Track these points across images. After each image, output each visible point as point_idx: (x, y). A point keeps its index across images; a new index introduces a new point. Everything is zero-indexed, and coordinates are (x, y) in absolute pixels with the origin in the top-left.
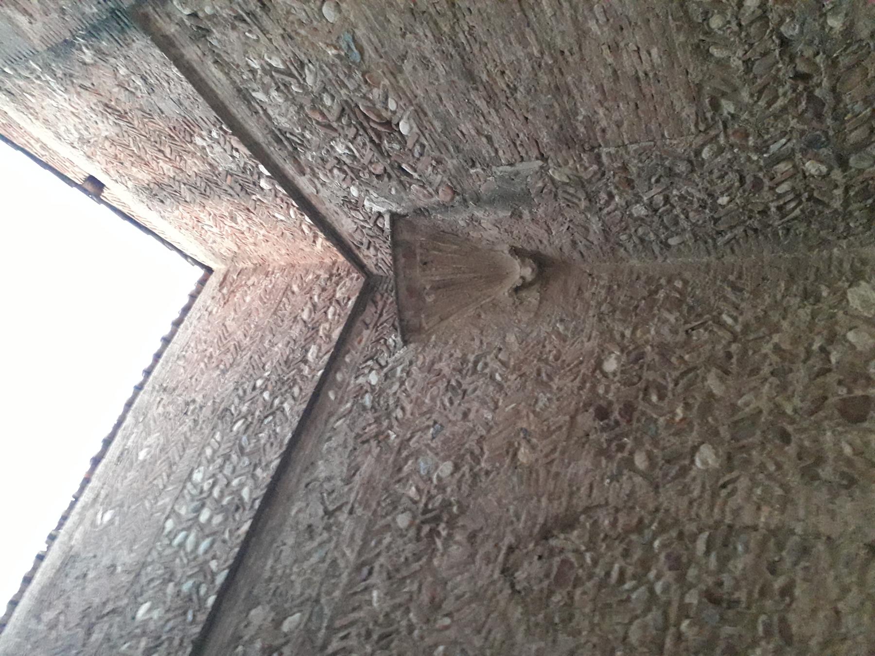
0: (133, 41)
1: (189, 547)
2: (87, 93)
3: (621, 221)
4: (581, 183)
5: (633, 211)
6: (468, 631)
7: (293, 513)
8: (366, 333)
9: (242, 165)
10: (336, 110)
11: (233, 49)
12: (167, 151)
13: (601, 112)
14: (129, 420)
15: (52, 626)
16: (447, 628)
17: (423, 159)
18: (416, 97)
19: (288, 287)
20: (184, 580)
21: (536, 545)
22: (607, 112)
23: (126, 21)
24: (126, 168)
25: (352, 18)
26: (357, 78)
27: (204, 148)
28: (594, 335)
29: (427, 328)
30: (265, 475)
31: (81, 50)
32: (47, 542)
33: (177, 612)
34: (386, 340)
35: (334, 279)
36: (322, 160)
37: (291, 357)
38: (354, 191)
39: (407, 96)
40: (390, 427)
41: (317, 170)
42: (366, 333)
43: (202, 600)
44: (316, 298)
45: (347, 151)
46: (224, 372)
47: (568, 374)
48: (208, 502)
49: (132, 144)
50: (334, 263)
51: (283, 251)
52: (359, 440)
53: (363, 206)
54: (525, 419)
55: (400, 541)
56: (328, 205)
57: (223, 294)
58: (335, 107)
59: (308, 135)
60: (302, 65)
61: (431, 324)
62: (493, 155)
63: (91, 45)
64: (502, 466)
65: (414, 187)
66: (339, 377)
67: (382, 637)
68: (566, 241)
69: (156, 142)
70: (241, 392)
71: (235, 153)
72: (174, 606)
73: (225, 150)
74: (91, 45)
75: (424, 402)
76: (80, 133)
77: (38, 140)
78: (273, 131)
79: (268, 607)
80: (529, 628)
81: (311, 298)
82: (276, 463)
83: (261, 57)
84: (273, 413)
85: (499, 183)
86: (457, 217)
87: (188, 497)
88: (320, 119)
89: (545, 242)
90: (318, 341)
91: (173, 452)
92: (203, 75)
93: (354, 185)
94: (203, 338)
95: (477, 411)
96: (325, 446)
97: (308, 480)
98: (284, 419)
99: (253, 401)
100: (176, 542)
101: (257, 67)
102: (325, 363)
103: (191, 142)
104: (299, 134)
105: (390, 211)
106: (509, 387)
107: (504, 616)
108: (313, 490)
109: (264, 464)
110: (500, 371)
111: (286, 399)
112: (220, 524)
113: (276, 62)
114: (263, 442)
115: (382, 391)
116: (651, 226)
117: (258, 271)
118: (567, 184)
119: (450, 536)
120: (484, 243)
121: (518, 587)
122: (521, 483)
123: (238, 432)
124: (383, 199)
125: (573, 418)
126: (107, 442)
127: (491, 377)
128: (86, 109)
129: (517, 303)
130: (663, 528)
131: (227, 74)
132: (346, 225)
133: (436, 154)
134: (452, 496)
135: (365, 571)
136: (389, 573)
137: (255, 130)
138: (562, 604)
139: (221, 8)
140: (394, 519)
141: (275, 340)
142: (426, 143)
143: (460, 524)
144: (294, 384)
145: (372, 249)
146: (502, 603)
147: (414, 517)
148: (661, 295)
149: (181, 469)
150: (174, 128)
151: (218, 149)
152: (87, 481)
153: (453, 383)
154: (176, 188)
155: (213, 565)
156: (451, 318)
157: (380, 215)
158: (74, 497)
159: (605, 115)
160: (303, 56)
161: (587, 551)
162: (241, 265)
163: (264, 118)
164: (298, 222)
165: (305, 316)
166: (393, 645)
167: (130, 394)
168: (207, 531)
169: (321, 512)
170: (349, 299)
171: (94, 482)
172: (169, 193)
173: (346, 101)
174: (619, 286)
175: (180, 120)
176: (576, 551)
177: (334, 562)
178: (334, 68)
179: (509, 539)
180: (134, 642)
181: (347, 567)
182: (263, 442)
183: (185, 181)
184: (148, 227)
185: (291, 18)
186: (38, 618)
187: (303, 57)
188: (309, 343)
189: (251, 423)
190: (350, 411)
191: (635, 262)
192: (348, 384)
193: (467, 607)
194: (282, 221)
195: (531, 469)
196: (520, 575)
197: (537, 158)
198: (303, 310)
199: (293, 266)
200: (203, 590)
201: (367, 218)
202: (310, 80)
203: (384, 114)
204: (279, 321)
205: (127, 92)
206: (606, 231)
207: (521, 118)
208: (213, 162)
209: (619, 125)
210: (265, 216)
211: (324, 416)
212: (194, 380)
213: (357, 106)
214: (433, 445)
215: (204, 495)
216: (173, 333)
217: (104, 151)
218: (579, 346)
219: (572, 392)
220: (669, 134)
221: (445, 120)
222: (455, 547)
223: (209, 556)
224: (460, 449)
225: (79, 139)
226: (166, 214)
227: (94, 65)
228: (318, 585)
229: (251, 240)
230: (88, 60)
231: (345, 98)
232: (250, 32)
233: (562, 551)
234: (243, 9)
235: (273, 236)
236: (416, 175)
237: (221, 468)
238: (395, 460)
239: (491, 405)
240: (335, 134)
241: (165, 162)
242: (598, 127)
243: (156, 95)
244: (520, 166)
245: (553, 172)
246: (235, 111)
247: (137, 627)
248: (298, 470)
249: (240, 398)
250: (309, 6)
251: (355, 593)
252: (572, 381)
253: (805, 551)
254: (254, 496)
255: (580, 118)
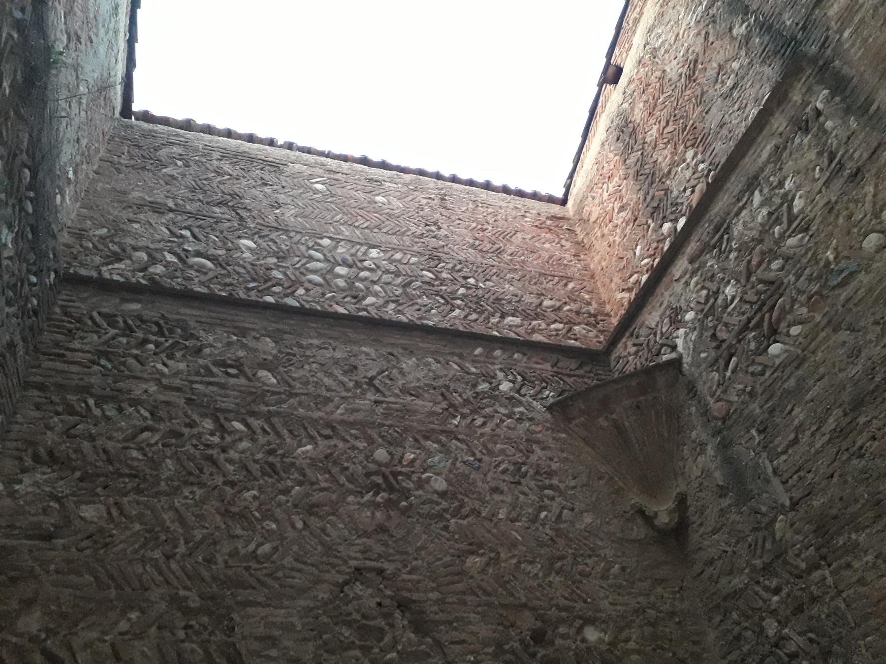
0: (770, 65)
1: (311, 265)
2: (702, 41)
3: (753, 609)
4: (780, 555)
5: (768, 620)
6: (295, 548)
7: (364, 349)
8: (548, 366)
9: (679, 201)
10: (771, 276)
11: (796, 159)
12: (670, 129)
13: (870, 558)
14: (408, 177)
15: (218, 172)
16: (293, 526)
17: (749, 377)
18: (813, 352)
19: (570, 279)
20: (281, 269)
21: (392, 598)
22: (870, 564)
23: (788, 53)
24: (641, 97)
25: (875, 266)
26: (811, 287)
27: (684, 161)
28: (619, 608)
29: (571, 426)
30: (390, 312)
31: (743, 22)
32: (285, 143)
33: (253, 272)
34: (546, 388)
35: (592, 320)
36: (713, 276)
37: (504, 302)
38: (690, 316)
39: (810, 344)
40: (464, 416)
41: (699, 273)
42: (548, 366)
43: (268, 291)
44: (567, 308)
45: (729, 298)
46: (473, 246)
47: (570, 590)
48: (354, 270)
49: (665, 95)
50: (608, 315)
51: (604, 264)
52: (444, 390)
53: (678, 329)
54: (510, 555)
55: (361, 457)
56: (667, 294)
57: (545, 222)
58: (772, 274)
59: (733, 255)
60: (806, 230)
61: (576, 429)
62: (779, 450)
63: (751, 30)
64: (456, 541)
65: (716, 375)
66: (498, 353)
67: (272, 466)
68: (712, 552)
69: (675, 116)
70: (459, 267)
71: (688, 191)
72: (258, 268)
73: (688, 181)
74: (751, 30)
75: (496, 443)
76: (660, 48)
77: (641, 14)
78: (725, 221)
79: (274, 352)
80: (312, 609)
81: (566, 303)
82: (403, 319)
83: (798, 188)
84: (447, 302)
85: (750, 464)
86: (699, 428)
87: (353, 251)
88: (754, 263)
89: (702, 530)
90: (525, 323)
91: (389, 225)
92: (759, 140)
93: (697, 314)
94: (499, 217)
95: (503, 501)
96: (430, 360)
97: (395, 353)
98: (444, 313)
99: (454, 280)
100: (312, 252)
101: (787, 186)
102: (507, 336)
103: (686, 148)
104: (731, 246)
105: (680, 357)
106: (537, 529)
107: (317, 581)
108: (389, 361)
109: (399, 308)
110: (550, 515)
111: (463, 310)
112: (337, 286)
113: (798, 204)
114: (419, 301)
115: (495, 398)
116: (757, 644)
117: (577, 246)
118: (774, 537)
119: (377, 506)
120: (681, 464)
121: (346, 588)
122: (446, 566)
123: (422, 276)
124: (692, 346)
125: (525, 606)
126: (384, 165)
127: (541, 507)
128: (686, 45)
129: (627, 516)
131: (768, 161)
132: (652, 317)
133: (759, 389)
134: (416, 497)
135: (328, 432)
136: (331, 454)
137: (720, 204)
138: (342, 638)
139: (836, 135)
140: (380, 445)
141: (515, 283)
142: (767, 374)
143: (392, 513)
144: (478, 313)
145: (635, 349)
146: (327, 576)
147: (386, 465)
149: (378, 237)
150: (695, 128)
151: (688, 174)
152: (345, 159)
153: (524, 469)
154: (636, 148)
155: (301, 291)
156: (590, 450)
157: (674, 348)
158: (329, 152)
159: (867, 563)
160: (814, 228)
161: (398, 652)
162: (578, 229)
163: (736, 209)
164: (638, 269)
165: (547, 303)
166: (266, 478)
167: (430, 169)
168: (328, 277)
169: (369, 375)
170: (576, 340)
171: (345, 166)
172: (628, 143)
173: (782, 283)
174: (680, 622)
175: (705, 131)
176: (395, 642)
177: (329, 400)
178: (813, 262)
179: (390, 568)
180: (220, 244)
181: (327, 413)
182: (419, 301)
183: (645, 154)
184: (590, 135)
185: (851, 206)
186: (222, 158)
187: (814, 228)
188: (521, 314)
189: (433, 286)
190: (468, 373)
191: (712, 636)
192: (493, 364)
193: (316, 541)
194: (635, 254)
195: (462, 573)
196: (358, 588)
197: (791, 499)
198: (551, 299)
199: (592, 277)
200: (276, 289)
201: (667, 335)
202: (791, 241)
203: (783, 325)
204: (534, 281)
205: (715, 75)
206: (735, 594)
207: (830, 471)
208: (673, 173)
209: (861, 582)
210: (634, 237)
211: (457, 351)
212: (459, 222)
213: (781, 296)
214: (458, 464)
215: (359, 264)
216: (495, 189)
217: (650, 74)
218: (601, 595)
219: (552, 599)
220: (870, 642)
221: (801, 388)
222: (369, 514)
223: (307, 285)
224: (461, 493)
225: (655, 48)
226: (607, 147)
227: (733, 38)
228: (306, 391)
229: (606, 231)
230: (735, 32)
231: (786, 281)
232: (821, 170)
233: (392, 626)
234: (843, 156)
235: (617, 251)
236: (728, 374)
237: (387, 272)
238: (433, 430)
239: (514, 515)
240: (743, 281)
241: (659, 129)
242: (850, 559)
243: (722, 102)
244: (776, 482)
245: (782, 520)
246: (733, 179)
247: (232, 242)
248: (402, 341)
249: (453, 268)
250: (871, 220)
251: (305, 429)
252: (563, 596)
254: (369, 308)
255: (854, 536)
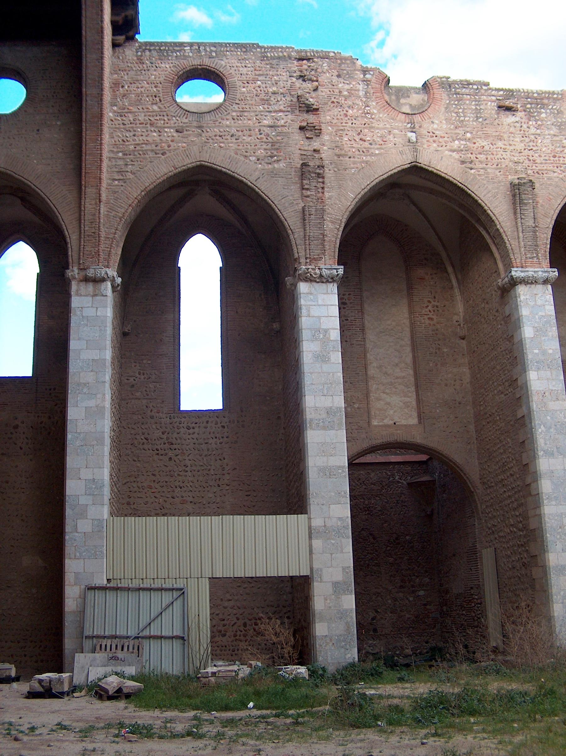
8: (410, 468)
130: (377, 555)
148: (425, 544)
179: (368, 527)
196: (363, 532)
253: (378, 577)
